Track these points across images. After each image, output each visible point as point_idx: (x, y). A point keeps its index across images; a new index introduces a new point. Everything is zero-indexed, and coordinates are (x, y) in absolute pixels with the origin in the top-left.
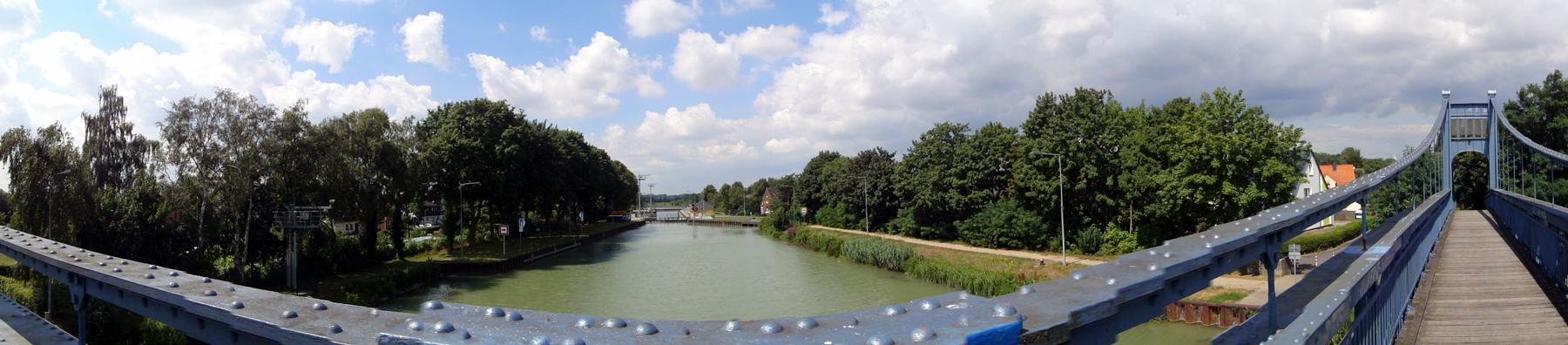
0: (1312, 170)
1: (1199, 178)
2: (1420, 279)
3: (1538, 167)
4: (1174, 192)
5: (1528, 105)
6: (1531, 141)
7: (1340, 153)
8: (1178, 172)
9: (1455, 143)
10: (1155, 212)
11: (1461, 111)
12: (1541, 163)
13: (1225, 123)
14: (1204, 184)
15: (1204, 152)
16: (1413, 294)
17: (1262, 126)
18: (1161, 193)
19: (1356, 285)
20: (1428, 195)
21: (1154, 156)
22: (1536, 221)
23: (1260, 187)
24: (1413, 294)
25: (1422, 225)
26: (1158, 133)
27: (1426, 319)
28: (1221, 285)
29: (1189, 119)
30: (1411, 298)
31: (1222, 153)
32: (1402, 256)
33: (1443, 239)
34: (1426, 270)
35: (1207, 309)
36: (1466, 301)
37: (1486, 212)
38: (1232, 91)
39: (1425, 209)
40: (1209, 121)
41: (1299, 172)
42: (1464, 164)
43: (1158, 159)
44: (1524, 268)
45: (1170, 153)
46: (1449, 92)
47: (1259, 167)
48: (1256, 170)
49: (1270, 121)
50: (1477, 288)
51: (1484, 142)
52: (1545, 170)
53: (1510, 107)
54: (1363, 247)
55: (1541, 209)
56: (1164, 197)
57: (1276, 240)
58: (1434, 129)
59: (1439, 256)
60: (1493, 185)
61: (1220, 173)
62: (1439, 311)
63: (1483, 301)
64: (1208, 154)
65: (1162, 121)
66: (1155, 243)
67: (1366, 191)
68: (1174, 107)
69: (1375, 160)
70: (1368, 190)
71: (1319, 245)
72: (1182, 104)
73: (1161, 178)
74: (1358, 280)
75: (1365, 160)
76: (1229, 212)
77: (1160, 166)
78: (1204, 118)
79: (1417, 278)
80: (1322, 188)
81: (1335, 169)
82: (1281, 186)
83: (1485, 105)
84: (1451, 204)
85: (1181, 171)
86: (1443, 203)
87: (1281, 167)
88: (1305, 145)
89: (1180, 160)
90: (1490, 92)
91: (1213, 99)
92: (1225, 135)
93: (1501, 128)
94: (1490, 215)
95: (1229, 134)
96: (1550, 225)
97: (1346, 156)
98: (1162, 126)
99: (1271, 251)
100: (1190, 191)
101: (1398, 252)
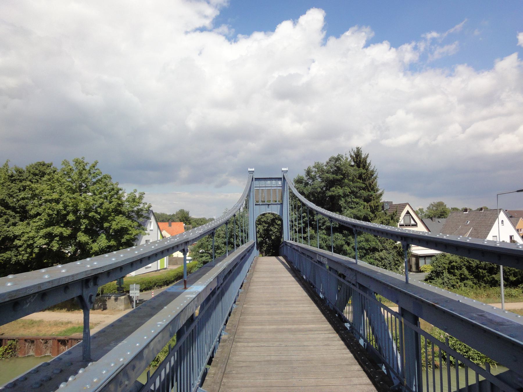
0: (152, 225)
1: (57, 230)
2: (232, 309)
3: (320, 224)
4: (31, 242)
5: (313, 179)
6: (314, 205)
7: (175, 213)
8: (36, 224)
9: (258, 207)
10: (10, 259)
11: (262, 183)
12: (321, 221)
13: (81, 186)
14: (61, 236)
15: (62, 208)
16: (227, 321)
17: (113, 189)
18: (17, 242)
19: (174, 318)
20: (238, 246)
21: (14, 209)
22: (319, 266)
23: (109, 238)
24: (227, 321)
25: (233, 268)
26: (20, 190)
27: (237, 342)
28: (70, 320)
29: (49, 180)
30: (225, 325)
31: (78, 211)
32: (218, 292)
33: (249, 278)
34: (236, 303)
35: (56, 342)
36: (268, 327)
37: (281, 258)
38: (89, 161)
39: (236, 256)
40: (68, 183)
41: (141, 227)
42: (265, 222)
43: (17, 212)
44: (312, 302)
45: (29, 207)
46: (253, 170)
47: (109, 222)
48: (106, 225)
49: (119, 186)
50: (276, 317)
51: (279, 206)
52: (325, 226)
53: (299, 181)
54: (183, 287)
55: (323, 256)
56: (20, 246)
57: (91, 284)
58: (243, 196)
59: (246, 292)
60: (287, 236)
61: (75, 226)
62: (246, 335)
63: (281, 327)
64: (65, 210)
65: (24, 180)
66: (505, 276)
67: (187, 243)
68: (37, 169)
69: (200, 219)
70: (188, 242)
71: (155, 284)
72: (45, 167)
73: (17, 230)
74: (176, 314)
75: (193, 219)
76: (61, 259)
77: (18, 219)
78: (64, 180)
79: (230, 309)
80: (160, 238)
81: (170, 225)
82: (126, 237)
83: (280, 179)
84: (256, 252)
85: (39, 223)
86: (249, 251)
87: (127, 223)
88: (146, 206)
89: (38, 214)
90: (283, 169)
91: (72, 165)
92: (81, 195)
93: (293, 196)
94: (284, 261)
95: (84, 195)
96: (330, 268)
97: (179, 216)
98: (24, 183)
99: (86, 294)
100: (47, 241)
101: (215, 289)
